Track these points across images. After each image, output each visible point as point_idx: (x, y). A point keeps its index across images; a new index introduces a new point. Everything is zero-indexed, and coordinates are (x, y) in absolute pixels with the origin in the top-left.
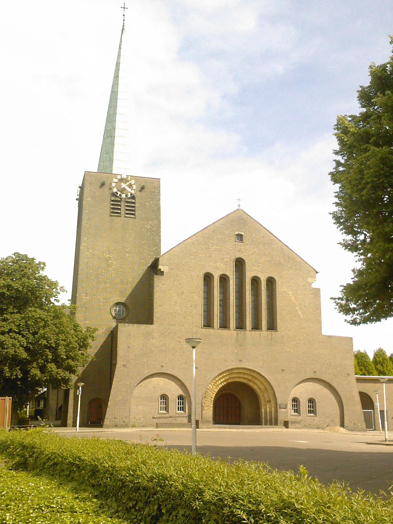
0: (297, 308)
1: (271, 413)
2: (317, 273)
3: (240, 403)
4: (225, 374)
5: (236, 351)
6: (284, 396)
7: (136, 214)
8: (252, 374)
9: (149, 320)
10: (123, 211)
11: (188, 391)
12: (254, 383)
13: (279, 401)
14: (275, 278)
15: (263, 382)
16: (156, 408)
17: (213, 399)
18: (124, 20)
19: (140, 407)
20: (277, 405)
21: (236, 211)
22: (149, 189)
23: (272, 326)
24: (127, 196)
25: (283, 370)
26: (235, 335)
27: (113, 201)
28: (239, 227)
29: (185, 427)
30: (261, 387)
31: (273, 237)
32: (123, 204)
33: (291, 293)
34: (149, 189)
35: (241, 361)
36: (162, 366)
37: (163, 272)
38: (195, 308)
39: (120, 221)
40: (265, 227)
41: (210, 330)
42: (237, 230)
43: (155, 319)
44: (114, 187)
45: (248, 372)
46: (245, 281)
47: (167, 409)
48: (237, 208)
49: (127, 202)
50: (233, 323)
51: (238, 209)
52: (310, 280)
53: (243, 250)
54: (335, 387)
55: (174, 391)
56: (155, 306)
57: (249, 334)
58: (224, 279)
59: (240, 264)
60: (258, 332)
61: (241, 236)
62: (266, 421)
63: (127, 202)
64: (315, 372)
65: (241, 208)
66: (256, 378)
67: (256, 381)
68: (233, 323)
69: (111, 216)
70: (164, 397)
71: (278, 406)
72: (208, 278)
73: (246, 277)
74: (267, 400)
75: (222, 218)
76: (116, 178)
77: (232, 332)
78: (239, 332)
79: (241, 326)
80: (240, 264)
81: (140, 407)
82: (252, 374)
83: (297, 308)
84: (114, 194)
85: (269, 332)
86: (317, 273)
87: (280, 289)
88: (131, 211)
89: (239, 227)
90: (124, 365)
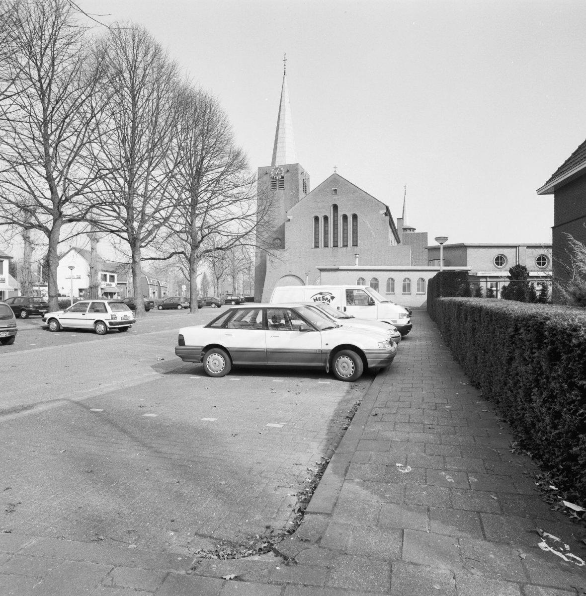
0: (372, 231)
10: (277, 187)
22: (293, 170)
23: (355, 244)
36: (290, 271)
48: (334, 173)
49: (280, 181)
50: (331, 243)
57: (341, 250)
58: (326, 218)
59: (335, 207)
61: (335, 190)
63: (280, 181)
80: (335, 207)
87: (360, 220)
89: (336, 184)
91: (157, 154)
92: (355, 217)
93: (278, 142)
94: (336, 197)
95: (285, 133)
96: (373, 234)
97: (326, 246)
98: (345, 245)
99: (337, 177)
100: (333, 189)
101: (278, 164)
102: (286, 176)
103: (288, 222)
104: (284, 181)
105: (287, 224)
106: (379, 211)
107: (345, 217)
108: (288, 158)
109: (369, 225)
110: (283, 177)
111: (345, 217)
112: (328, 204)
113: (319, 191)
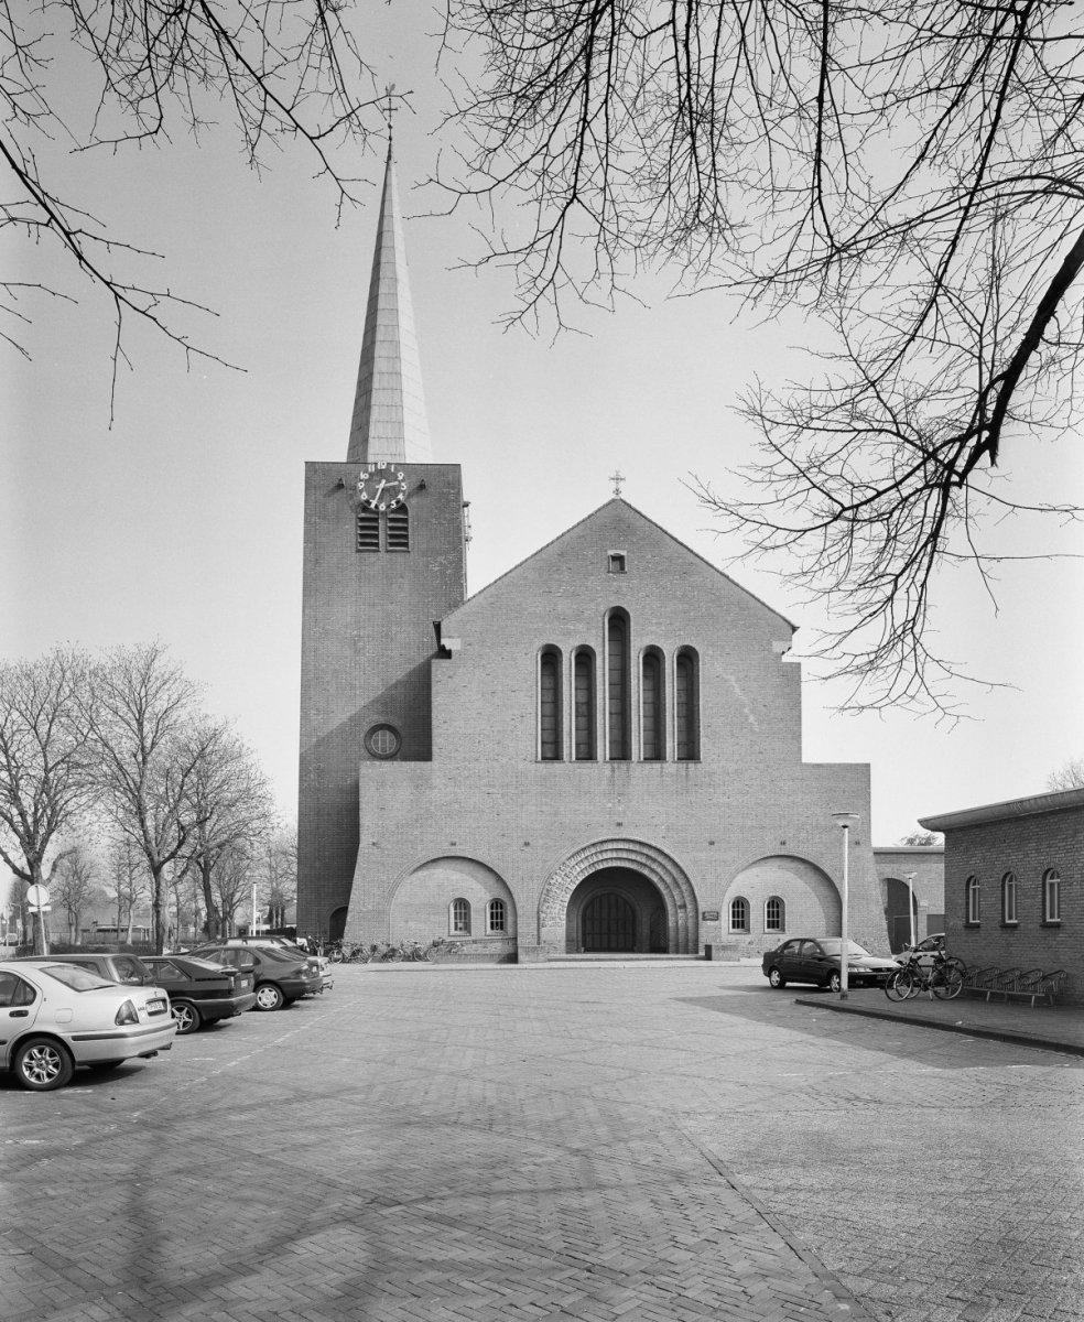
0: (746, 710)
1: (686, 928)
2: (794, 629)
3: (633, 912)
4: (588, 853)
5: (610, 805)
6: (716, 896)
7: (411, 542)
8: (645, 851)
9: (425, 754)
10: (382, 540)
11: (510, 893)
12: (653, 870)
13: (702, 907)
14: (697, 648)
15: (669, 867)
16: (443, 926)
17: (566, 905)
18: (390, 139)
19: (411, 924)
20: (697, 912)
21: (609, 504)
22: (440, 488)
23: (690, 752)
24: (388, 507)
25: (712, 843)
26: (608, 772)
27: (362, 519)
28: (617, 538)
29: (483, 962)
30: (668, 880)
31: (691, 558)
32: (381, 523)
33: (733, 678)
34: (440, 488)
35: (619, 824)
36: (453, 844)
37: (450, 651)
38: (522, 722)
39: (380, 560)
40: (675, 536)
41: (556, 766)
42: (612, 547)
43: (435, 749)
44: (361, 491)
45: (637, 848)
46: (630, 658)
47: (467, 928)
48: (614, 496)
49: (392, 520)
50: (603, 747)
51: (614, 500)
52: (777, 647)
53: (625, 589)
54: (825, 870)
55: (480, 895)
56: (434, 723)
57: (640, 771)
58: (585, 657)
59: (619, 621)
60: (657, 765)
61: (619, 559)
62: (677, 945)
63: (392, 520)
64: (783, 843)
65: (622, 496)
66: (654, 860)
67: (654, 866)
68: (603, 747)
69: (358, 551)
70: (462, 905)
71: (700, 917)
72: (551, 657)
73: (632, 649)
74: (678, 904)
75: (578, 524)
76: (366, 471)
77: (601, 768)
78: (616, 765)
79: (622, 753)
80: (619, 621)
81: (411, 924)
82: (645, 851)
83: (746, 710)
84: (365, 507)
85: (682, 766)
86: (794, 629)
87: (706, 670)
88: (400, 539)
89: (617, 538)
90: (374, 844)
91: (106, 714)
92: (687, 658)
93: (376, 385)
94: (621, 582)
95: (398, 357)
96: (751, 719)
97: (656, 754)
98: (587, 753)
99: (628, 514)
100: (611, 552)
101: (378, 454)
102: (412, 504)
103: (445, 663)
104: (406, 521)
105: (440, 668)
106: (770, 644)
107: (653, 657)
108: (415, 440)
109: (737, 690)
110: (402, 508)
111: (653, 657)
112: (592, 606)
113: (561, 555)
